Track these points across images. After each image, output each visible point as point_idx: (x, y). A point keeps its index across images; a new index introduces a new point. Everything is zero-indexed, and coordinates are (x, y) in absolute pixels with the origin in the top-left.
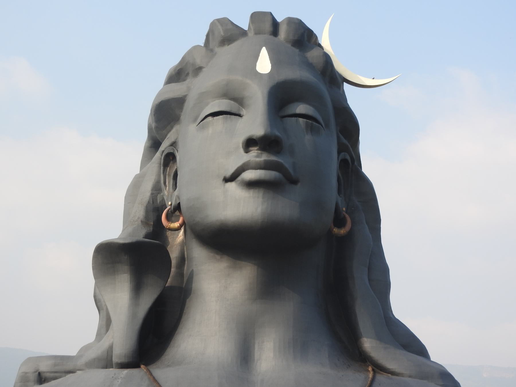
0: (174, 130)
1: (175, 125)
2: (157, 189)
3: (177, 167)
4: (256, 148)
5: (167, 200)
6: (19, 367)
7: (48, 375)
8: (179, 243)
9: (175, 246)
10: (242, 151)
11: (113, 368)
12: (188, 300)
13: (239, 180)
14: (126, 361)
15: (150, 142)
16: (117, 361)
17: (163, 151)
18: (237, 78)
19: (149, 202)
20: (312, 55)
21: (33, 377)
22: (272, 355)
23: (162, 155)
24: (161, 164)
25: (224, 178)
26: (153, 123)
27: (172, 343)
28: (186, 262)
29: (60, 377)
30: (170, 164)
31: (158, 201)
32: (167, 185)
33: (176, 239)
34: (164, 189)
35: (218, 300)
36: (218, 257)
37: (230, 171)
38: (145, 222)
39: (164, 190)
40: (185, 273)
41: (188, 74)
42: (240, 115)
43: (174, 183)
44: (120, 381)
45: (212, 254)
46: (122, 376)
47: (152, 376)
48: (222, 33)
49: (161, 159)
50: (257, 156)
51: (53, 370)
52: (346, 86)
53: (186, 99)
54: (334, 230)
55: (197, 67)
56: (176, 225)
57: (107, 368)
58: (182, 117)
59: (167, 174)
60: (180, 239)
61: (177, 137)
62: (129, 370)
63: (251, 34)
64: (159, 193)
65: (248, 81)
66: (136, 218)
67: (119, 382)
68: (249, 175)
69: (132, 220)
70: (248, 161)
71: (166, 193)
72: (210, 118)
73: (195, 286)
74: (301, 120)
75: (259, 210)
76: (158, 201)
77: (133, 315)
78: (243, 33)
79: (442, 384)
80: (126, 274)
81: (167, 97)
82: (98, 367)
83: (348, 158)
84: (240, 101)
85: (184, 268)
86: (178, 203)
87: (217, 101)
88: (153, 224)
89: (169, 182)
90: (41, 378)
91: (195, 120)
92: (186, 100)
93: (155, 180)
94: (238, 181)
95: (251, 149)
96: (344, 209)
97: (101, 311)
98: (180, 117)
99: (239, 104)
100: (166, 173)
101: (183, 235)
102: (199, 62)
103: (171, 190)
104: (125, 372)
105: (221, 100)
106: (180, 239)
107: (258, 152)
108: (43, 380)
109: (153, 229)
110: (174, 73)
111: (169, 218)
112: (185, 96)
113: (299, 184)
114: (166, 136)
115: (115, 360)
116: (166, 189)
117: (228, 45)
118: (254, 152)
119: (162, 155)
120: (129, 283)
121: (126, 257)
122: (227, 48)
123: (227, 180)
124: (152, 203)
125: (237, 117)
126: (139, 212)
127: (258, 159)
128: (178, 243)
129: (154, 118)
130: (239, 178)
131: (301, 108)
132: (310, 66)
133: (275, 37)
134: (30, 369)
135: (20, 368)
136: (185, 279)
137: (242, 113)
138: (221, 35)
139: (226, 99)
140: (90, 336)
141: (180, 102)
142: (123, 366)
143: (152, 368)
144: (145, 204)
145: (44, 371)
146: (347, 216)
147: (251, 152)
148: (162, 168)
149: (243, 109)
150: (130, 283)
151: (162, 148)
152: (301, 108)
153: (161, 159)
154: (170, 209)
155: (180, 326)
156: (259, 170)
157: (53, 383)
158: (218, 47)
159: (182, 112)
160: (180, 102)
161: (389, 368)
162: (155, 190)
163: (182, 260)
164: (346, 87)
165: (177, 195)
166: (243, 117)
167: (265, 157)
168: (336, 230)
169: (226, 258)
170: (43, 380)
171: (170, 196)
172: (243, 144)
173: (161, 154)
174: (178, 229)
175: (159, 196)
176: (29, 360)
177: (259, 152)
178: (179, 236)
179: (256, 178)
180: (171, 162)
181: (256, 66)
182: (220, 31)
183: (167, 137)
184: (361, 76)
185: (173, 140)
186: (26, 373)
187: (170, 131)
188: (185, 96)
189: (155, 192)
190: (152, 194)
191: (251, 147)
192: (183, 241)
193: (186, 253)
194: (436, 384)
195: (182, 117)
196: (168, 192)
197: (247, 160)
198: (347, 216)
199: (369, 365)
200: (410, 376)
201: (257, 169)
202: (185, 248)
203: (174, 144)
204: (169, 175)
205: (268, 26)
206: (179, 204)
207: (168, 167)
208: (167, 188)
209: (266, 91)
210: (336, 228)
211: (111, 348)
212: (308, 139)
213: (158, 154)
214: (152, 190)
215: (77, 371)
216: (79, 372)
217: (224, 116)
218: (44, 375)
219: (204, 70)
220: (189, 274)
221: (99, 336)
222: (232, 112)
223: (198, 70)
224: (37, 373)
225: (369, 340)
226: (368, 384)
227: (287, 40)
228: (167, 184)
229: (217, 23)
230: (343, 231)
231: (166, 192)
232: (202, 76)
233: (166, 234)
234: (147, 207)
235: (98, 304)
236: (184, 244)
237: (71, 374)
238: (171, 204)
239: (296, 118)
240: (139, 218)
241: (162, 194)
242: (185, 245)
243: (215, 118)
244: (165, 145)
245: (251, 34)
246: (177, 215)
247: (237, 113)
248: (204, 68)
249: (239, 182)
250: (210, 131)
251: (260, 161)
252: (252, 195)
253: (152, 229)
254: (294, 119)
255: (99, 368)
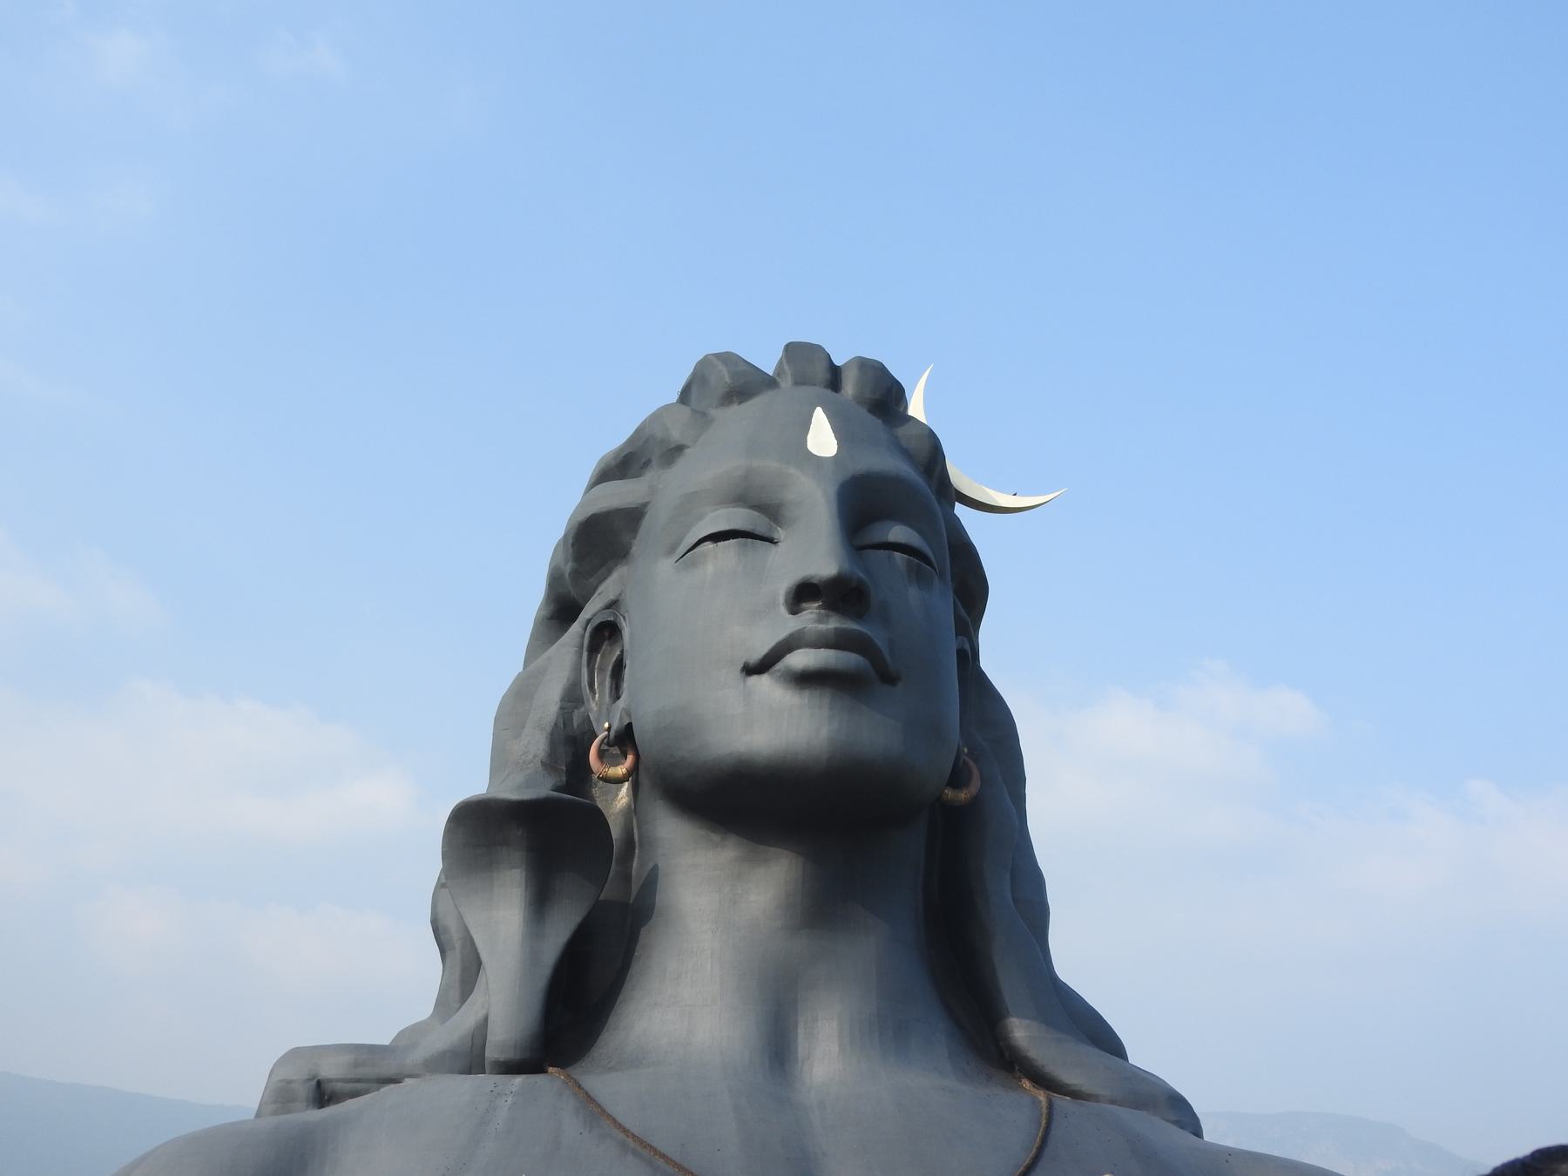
0: (615, 576)
1: (616, 566)
2: (573, 698)
3: (622, 651)
4: (817, 605)
5: (598, 720)
6: (271, 1068)
7: (339, 1086)
8: (621, 811)
9: (613, 817)
10: (783, 610)
11: (485, 1073)
12: (643, 931)
13: (778, 671)
14: (518, 1057)
15: (552, 607)
16: (496, 1056)
17: (589, 621)
18: (769, 464)
19: (556, 724)
20: (902, 431)
21: (304, 1091)
22: (835, 1048)
23: (585, 629)
24: (581, 647)
25: (744, 666)
26: (566, 564)
27: (610, 1020)
28: (637, 851)
29: (367, 1092)
30: (604, 647)
31: (575, 724)
32: (597, 691)
33: (612, 803)
34: (591, 699)
35: (717, 928)
36: (716, 838)
37: (760, 648)
38: (549, 764)
39: (588, 701)
40: (633, 873)
41: (647, 464)
42: (771, 541)
43: (614, 686)
44: (510, 1100)
45: (702, 832)
46: (514, 1089)
47: (583, 1089)
48: (727, 379)
49: (583, 636)
50: (820, 621)
51: (349, 1077)
52: (960, 510)
53: (646, 510)
54: (946, 791)
55: (673, 446)
56: (620, 770)
57: (470, 1073)
58: (634, 548)
59: (596, 666)
60: (621, 802)
61: (622, 591)
62: (524, 1076)
63: (786, 383)
64: (576, 708)
65: (792, 471)
66: (530, 757)
67: (509, 1102)
68: (800, 659)
69: (521, 761)
70: (800, 630)
71: (593, 706)
72: (709, 546)
73: (660, 898)
74: (897, 555)
75: (824, 732)
76: (575, 724)
77: (532, 957)
78: (770, 383)
79: (1174, 1118)
80: (518, 870)
81: (604, 505)
82: (452, 1072)
83: (967, 647)
84: (773, 511)
85: (632, 862)
86: (626, 723)
87: (722, 511)
88: (567, 770)
89: (601, 684)
90: (323, 1095)
91: (671, 551)
92: (646, 513)
93: (568, 680)
94: (775, 671)
95: (804, 605)
96: (966, 750)
97: (449, 954)
98: (631, 548)
99: (770, 518)
100: (595, 665)
101: (627, 796)
102: (676, 435)
103: (607, 698)
104: (518, 1080)
105: (731, 509)
106: (621, 802)
107: (819, 613)
108: (326, 1098)
109: (567, 781)
110: (613, 463)
111: (601, 754)
112: (645, 505)
113: (900, 685)
114: (595, 589)
115: (491, 1054)
116: (594, 698)
117: (740, 403)
118: (812, 613)
119: (585, 629)
120: (524, 889)
121: (519, 834)
122: (736, 411)
123: (751, 670)
124: (562, 727)
125: (768, 543)
126: (535, 743)
127: (822, 627)
128: (617, 810)
129: (571, 551)
130: (780, 666)
131: (898, 533)
132: (906, 454)
133: (833, 393)
134: (297, 1073)
135: (272, 1071)
136: (635, 888)
137: (776, 536)
138: (726, 383)
139: (744, 507)
140: (422, 1007)
141: (633, 517)
142: (510, 1068)
143: (576, 1071)
144: (549, 729)
145: (331, 1077)
146: (972, 764)
147: (805, 612)
148: (585, 654)
149: (779, 528)
150: (526, 887)
151: (585, 615)
152: (898, 533)
153: (583, 636)
154: (605, 738)
155: (627, 986)
156: (822, 650)
157: (350, 1105)
158: (716, 407)
159: (635, 538)
160: (633, 517)
161: (1067, 1084)
162: (569, 701)
163: (629, 843)
164: (960, 510)
165: (623, 708)
166: (779, 544)
167: (833, 624)
168: (949, 793)
169: (732, 840)
170: (326, 1098)
171: (604, 711)
172: (787, 594)
173: (584, 625)
174: (619, 781)
175: (576, 712)
176: (295, 1054)
177: (823, 611)
178: (620, 796)
179: (818, 666)
180: (606, 643)
181: (806, 442)
182: (723, 377)
183: (597, 594)
184: (994, 489)
185: (612, 597)
186: (290, 1082)
187: (605, 578)
188: (645, 505)
189: (569, 704)
190: (562, 708)
191: (804, 602)
192: (628, 808)
193: (636, 831)
194: (1163, 1119)
195: (635, 550)
196: (600, 705)
197: (797, 629)
198: (972, 764)
199: (1020, 1078)
200: (1113, 1102)
201: (820, 648)
202: (635, 822)
203: (613, 605)
204: (602, 670)
205: (821, 373)
206: (630, 726)
207: (599, 653)
208: (597, 696)
209: (833, 489)
210: (949, 788)
211: (483, 1025)
212: (913, 594)
213: (576, 627)
214: (562, 700)
215: (406, 1079)
216: (408, 1081)
217: (740, 539)
218: (328, 1088)
219: (687, 451)
220: (645, 874)
221: (444, 1007)
222: (757, 533)
223: (674, 452)
224: (314, 1083)
225: (1026, 1022)
226: (1044, 1115)
227: (859, 400)
228: (596, 687)
229: (715, 360)
230: (963, 796)
231: (593, 706)
232: (681, 464)
233: (591, 792)
234: (552, 734)
235: (442, 936)
236: (634, 810)
237: (392, 1086)
238: (609, 729)
239: (887, 552)
240: (535, 756)
241: (582, 709)
242: (635, 814)
243: (721, 544)
244: (592, 609)
245: (786, 383)
246: (614, 754)
247: (767, 535)
248: (688, 447)
249: (779, 675)
250: (710, 568)
251: (827, 630)
252: (806, 701)
253: (564, 778)
254: (882, 553)
255: (453, 1072)
